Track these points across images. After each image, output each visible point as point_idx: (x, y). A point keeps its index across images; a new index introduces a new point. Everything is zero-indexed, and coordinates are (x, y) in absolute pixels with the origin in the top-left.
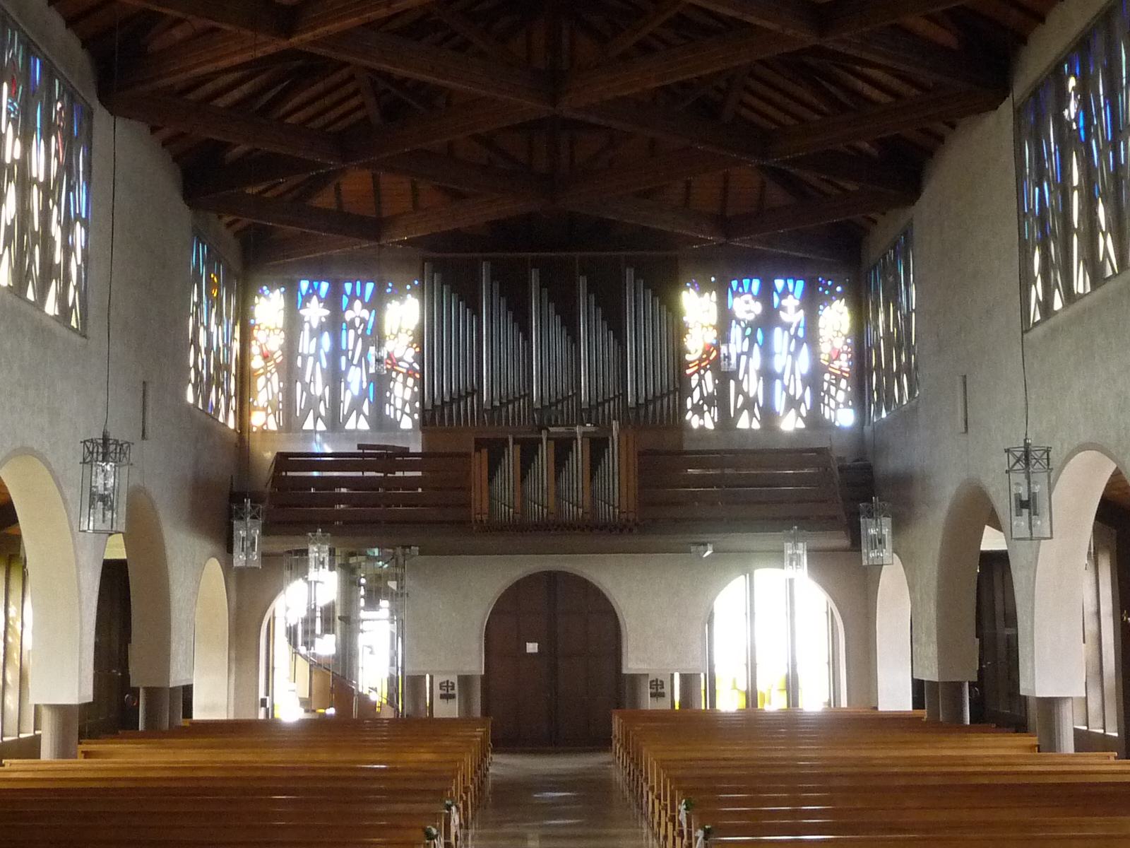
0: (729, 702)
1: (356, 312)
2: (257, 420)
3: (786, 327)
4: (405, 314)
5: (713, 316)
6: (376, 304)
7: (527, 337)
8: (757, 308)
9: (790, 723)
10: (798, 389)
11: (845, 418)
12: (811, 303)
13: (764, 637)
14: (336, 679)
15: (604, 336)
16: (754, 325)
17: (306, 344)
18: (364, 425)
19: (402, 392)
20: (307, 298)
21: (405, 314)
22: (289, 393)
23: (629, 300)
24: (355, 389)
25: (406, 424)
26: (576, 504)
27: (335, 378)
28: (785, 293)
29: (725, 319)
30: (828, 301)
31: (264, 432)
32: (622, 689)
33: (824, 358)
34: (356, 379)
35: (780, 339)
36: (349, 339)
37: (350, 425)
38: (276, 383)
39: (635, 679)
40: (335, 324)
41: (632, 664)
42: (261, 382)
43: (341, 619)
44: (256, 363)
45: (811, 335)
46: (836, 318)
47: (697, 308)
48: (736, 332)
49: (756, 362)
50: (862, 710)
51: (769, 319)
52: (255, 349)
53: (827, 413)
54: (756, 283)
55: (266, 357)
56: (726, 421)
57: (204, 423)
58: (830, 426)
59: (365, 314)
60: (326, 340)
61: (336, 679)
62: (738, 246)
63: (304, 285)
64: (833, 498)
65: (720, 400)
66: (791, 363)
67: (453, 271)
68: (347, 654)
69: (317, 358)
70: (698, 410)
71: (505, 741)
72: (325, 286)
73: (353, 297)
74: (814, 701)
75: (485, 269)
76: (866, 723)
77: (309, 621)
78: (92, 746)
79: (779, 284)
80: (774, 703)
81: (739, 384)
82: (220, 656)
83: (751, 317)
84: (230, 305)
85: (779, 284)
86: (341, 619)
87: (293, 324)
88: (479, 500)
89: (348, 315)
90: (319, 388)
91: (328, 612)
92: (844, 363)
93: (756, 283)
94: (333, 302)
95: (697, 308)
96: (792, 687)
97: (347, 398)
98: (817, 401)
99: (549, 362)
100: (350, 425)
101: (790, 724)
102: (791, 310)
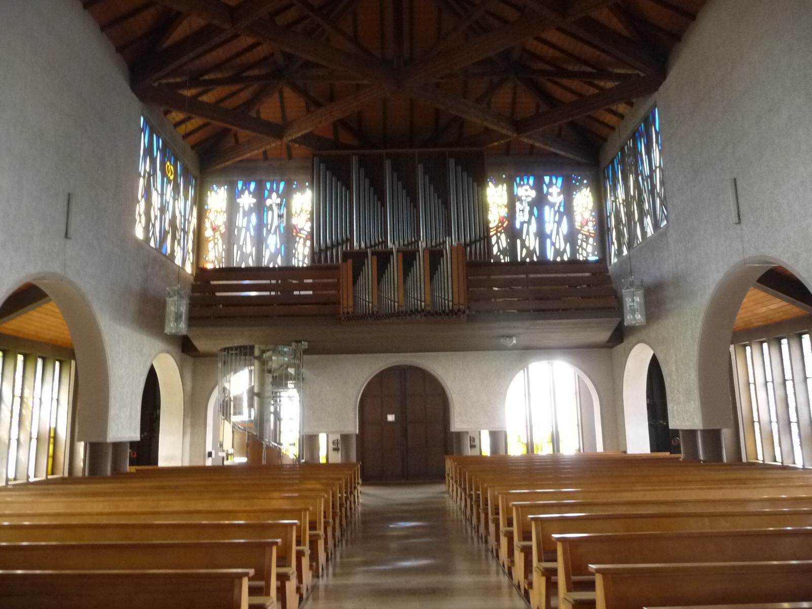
3: (552, 205)
4: (304, 201)
5: (505, 200)
8: (533, 194)
12: (568, 191)
13: (536, 405)
17: (241, 221)
20: (242, 192)
28: (550, 185)
35: (549, 214)
38: (221, 246)
42: (211, 245)
44: (208, 233)
46: (584, 200)
49: (533, 228)
51: (540, 202)
52: (207, 224)
55: (214, 229)
60: (254, 218)
69: (248, 229)
71: (370, 479)
72: (253, 186)
80: (544, 449)
88: (347, 304)
95: (495, 196)
96: (555, 441)
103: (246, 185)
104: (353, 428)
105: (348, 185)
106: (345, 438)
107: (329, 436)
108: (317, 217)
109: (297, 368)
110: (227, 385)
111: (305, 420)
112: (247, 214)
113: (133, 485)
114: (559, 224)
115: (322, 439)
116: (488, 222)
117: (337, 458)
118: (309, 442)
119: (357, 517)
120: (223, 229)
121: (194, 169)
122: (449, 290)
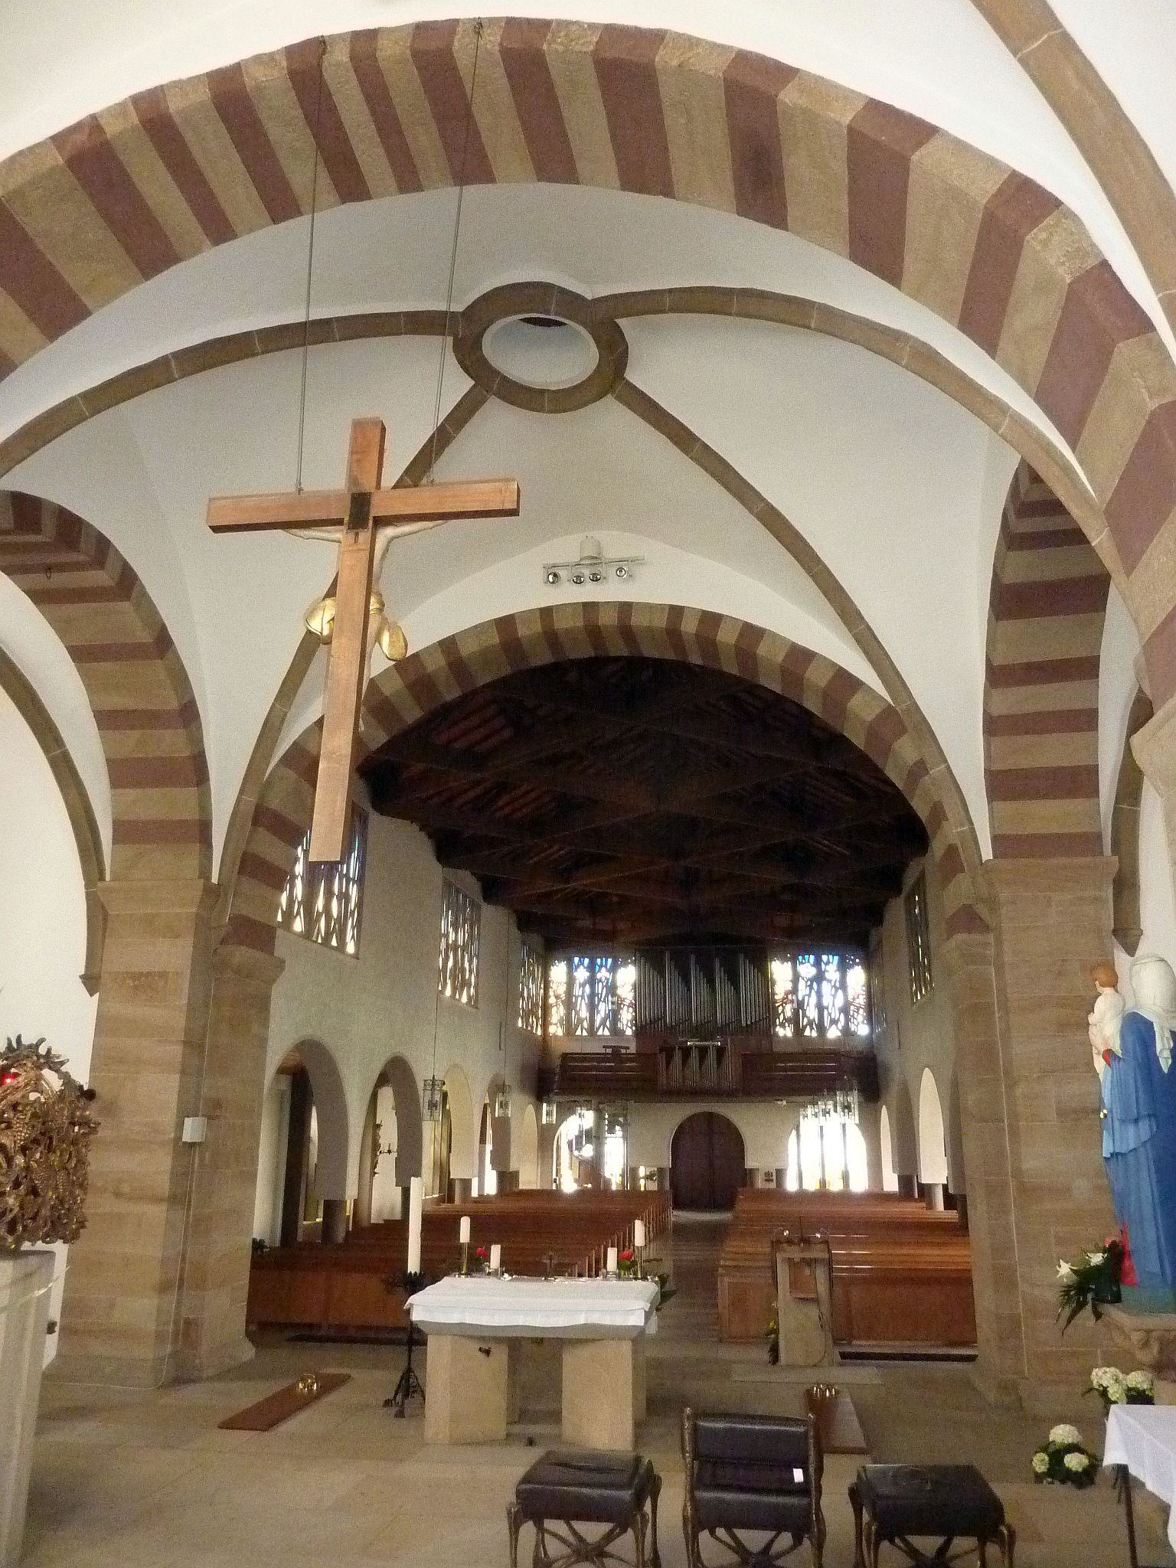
0: (791, 1185)
1: (603, 974)
2: (552, 1030)
3: (830, 981)
4: (628, 976)
5: (789, 975)
6: (613, 970)
7: (689, 990)
8: (813, 971)
9: (845, 1196)
10: (835, 1014)
11: (862, 1029)
12: (843, 967)
13: (822, 1151)
14: (592, 1170)
15: (729, 989)
16: (812, 980)
17: (577, 991)
18: (607, 1033)
19: (627, 1016)
20: (578, 967)
21: (628, 976)
22: (568, 1015)
23: (742, 973)
24: (602, 1014)
25: (629, 1032)
26: (711, 1081)
27: (592, 1008)
28: (828, 963)
29: (796, 978)
30: (851, 967)
31: (555, 1036)
32: (748, 1175)
33: (850, 998)
34: (603, 1008)
35: (826, 987)
36: (599, 988)
37: (600, 1033)
38: (562, 1011)
39: (752, 1172)
40: (592, 981)
41: (750, 1163)
42: (554, 1010)
43: (594, 1136)
44: (552, 1000)
45: (843, 985)
46: (857, 976)
47: (780, 971)
48: (802, 985)
49: (813, 1000)
50: (877, 1190)
51: (819, 978)
52: (551, 993)
53: (853, 1028)
54: (812, 957)
55: (557, 997)
56: (798, 1031)
57: (528, 1035)
58: (854, 1034)
59: (607, 975)
60: (588, 989)
61: (592, 1170)
62: (801, 940)
63: (576, 959)
64: (859, 1076)
65: (795, 1020)
66: (833, 1001)
67: (650, 955)
68: (599, 1156)
69: (583, 997)
70: (782, 1025)
71: (678, 1205)
72: (587, 961)
73: (601, 966)
74: (860, 1184)
75: (667, 955)
76: (877, 1196)
77: (579, 1138)
78: (951, 1252)
79: (824, 958)
80: (835, 1186)
81: (804, 1011)
82: (533, 1154)
83: (810, 976)
84: (538, 972)
85: (824, 958)
86: (594, 1136)
87: (571, 982)
88: (663, 1079)
89: (599, 976)
90: (584, 1013)
91: (588, 1133)
92: (862, 1000)
93: (812, 957)
94: (592, 968)
95: (780, 971)
96: (846, 1177)
97: (598, 1019)
98: (847, 1020)
99: (703, 1000)
100: (600, 1033)
101: (845, 1197)
102: (832, 971)
103: (581, 963)
104: (667, 1163)
105: (662, 974)
106: (661, 1170)
107: (374, 484)
108: (637, 987)
109: (625, 1116)
110: (813, 1312)
111: (628, 1156)
112: (582, 985)
113: (1144, 1174)
114: (834, 996)
115: (642, 1171)
116: (774, 994)
117: (653, 1186)
118: (631, 1173)
119: (670, 1226)
120: (563, 997)
121: (540, 950)
122: (732, 1067)
